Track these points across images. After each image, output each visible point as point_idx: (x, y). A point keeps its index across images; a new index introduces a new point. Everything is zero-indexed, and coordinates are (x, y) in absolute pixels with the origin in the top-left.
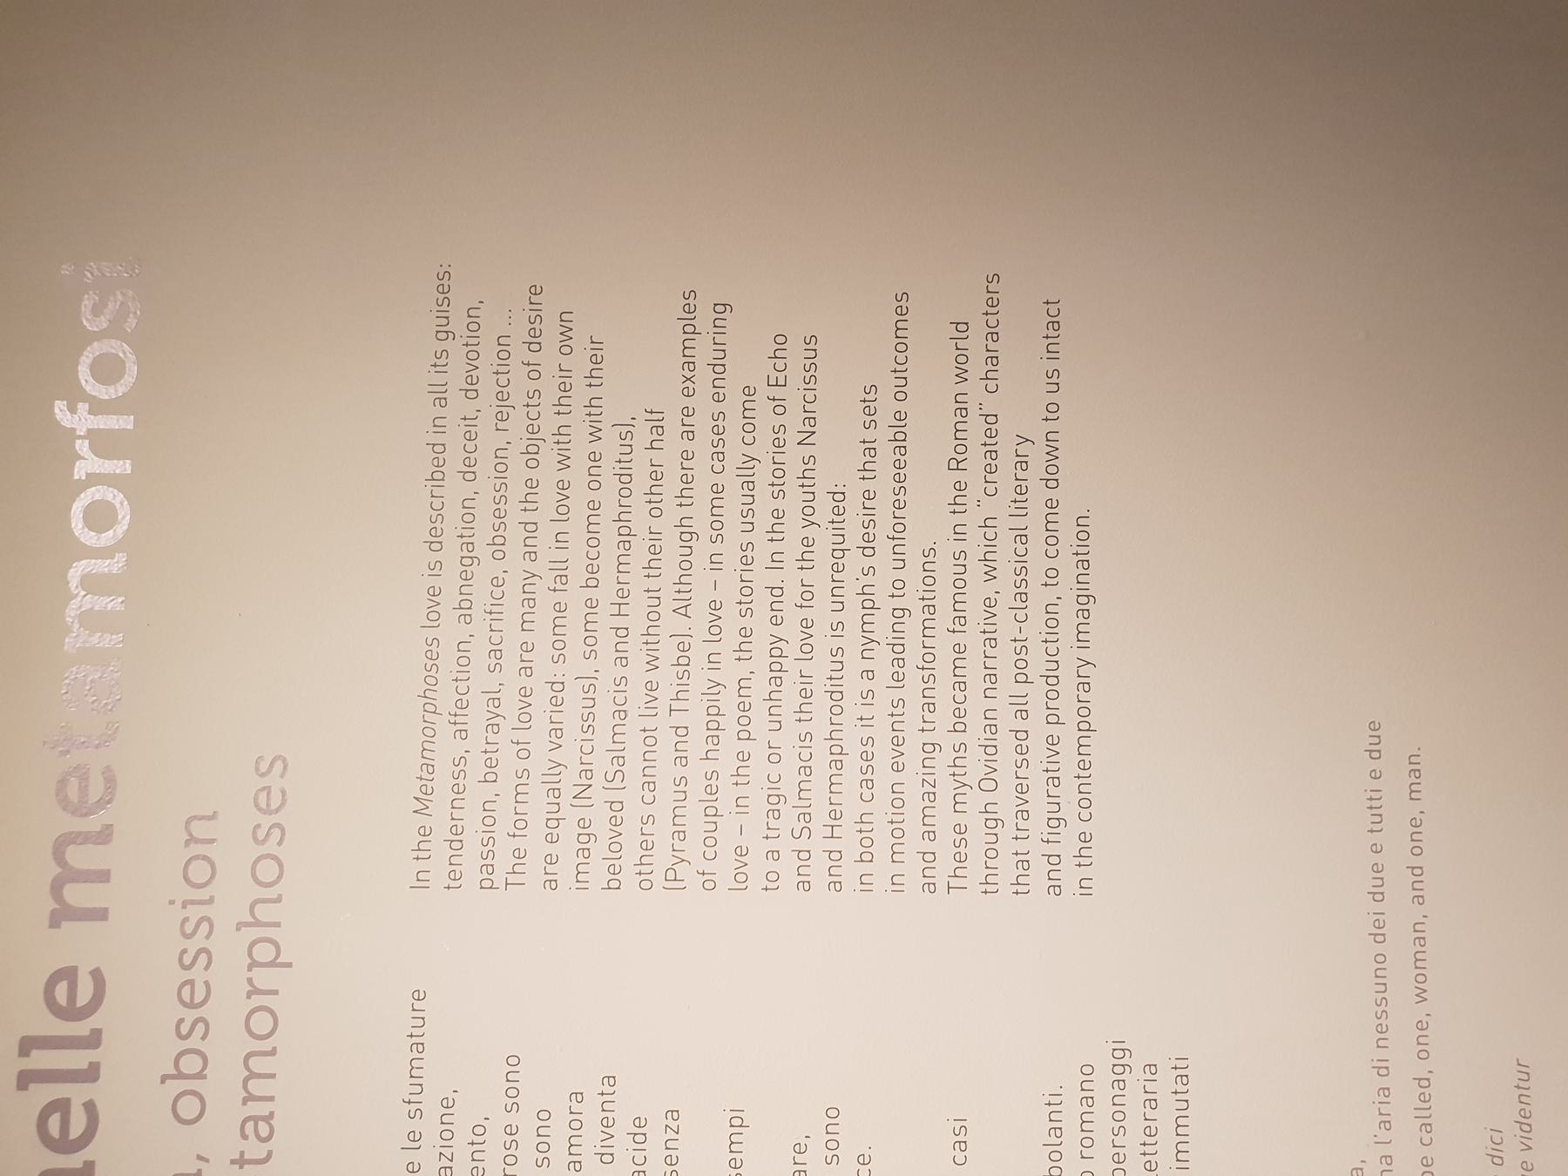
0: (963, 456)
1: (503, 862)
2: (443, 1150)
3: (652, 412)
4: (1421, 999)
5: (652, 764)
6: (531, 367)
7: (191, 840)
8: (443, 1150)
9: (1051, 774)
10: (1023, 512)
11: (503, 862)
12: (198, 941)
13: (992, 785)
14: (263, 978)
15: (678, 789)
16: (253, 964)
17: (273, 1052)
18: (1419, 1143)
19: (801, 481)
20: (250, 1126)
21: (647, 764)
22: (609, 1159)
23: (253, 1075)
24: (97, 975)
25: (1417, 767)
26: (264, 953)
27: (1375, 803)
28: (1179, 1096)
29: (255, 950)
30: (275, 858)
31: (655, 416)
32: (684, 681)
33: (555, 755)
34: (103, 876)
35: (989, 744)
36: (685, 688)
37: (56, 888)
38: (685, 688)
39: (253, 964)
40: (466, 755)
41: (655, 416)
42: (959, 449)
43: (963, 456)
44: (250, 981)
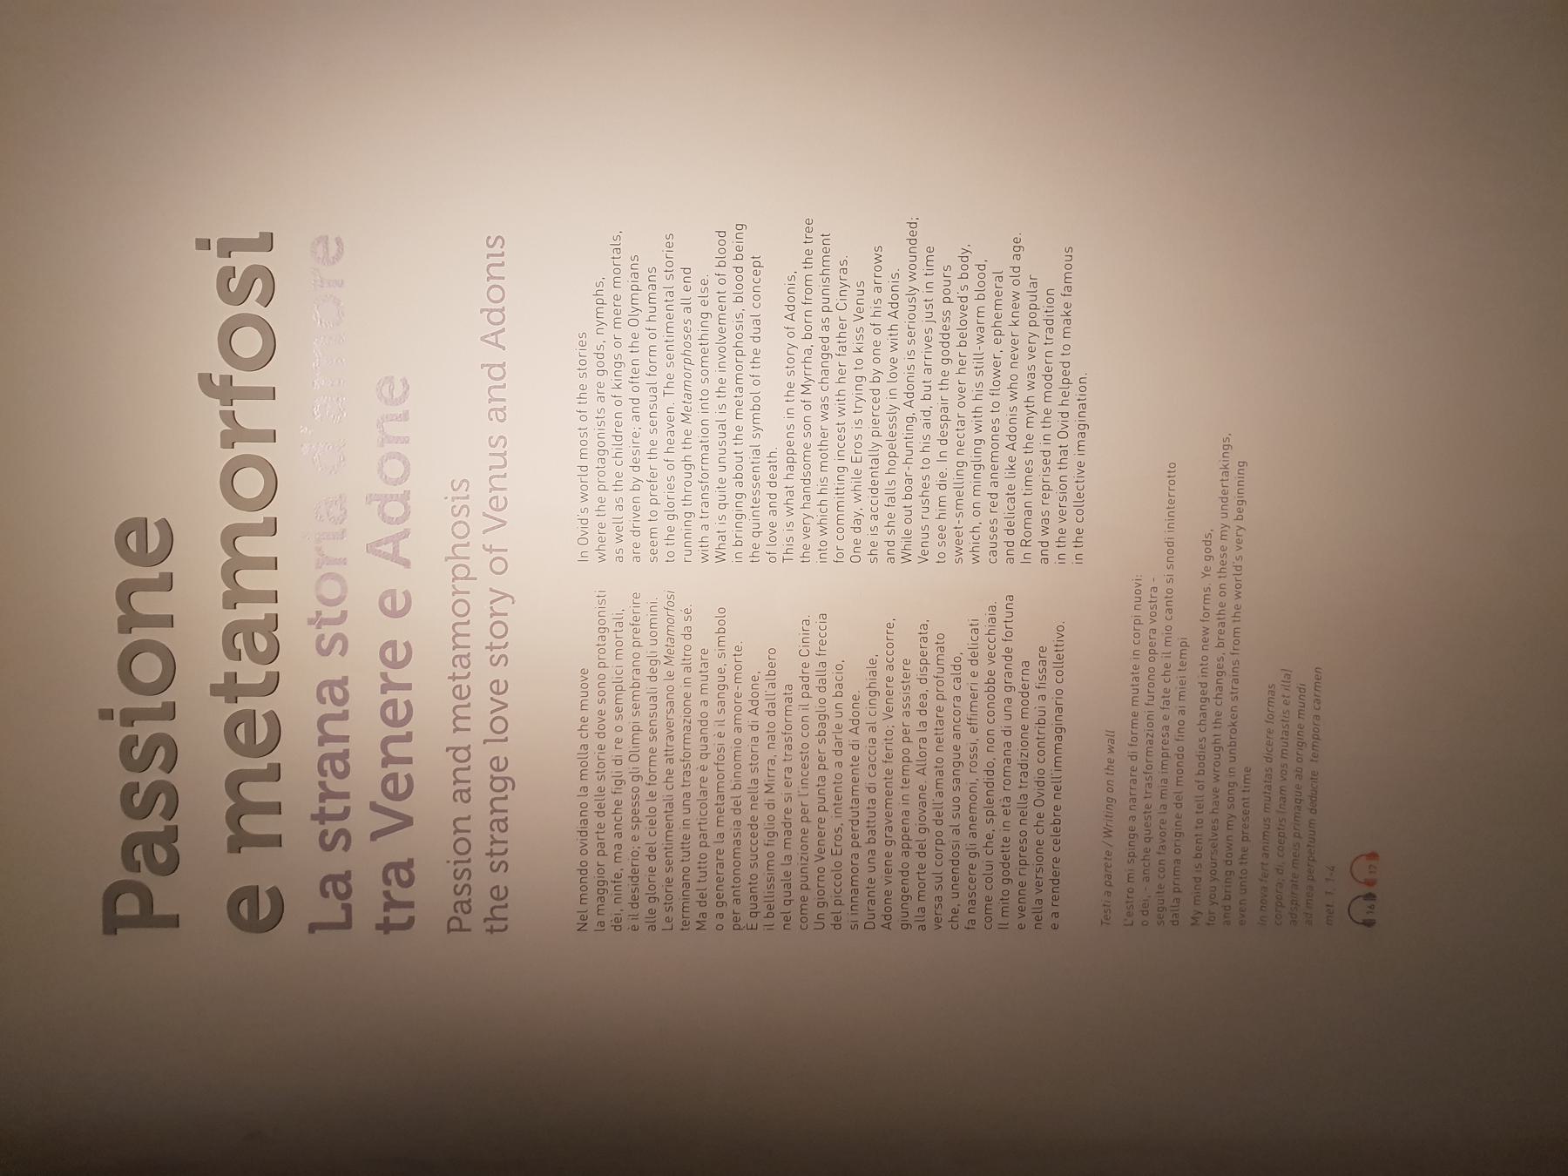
5: (827, 268)
7: (457, 831)
9: (974, 627)
12: (464, 881)
13: (857, 559)
14: (460, 585)
16: (455, 578)
20: (458, 795)
21: (825, 268)
22: (924, 713)
23: (458, 718)
24: (407, 645)
26: (461, 572)
27: (702, 865)
28: (703, 674)
29: (457, 845)
30: (465, 523)
33: (912, 284)
36: (1014, 417)
38: (1014, 417)
39: (455, 578)
40: (620, 234)
42: (704, 476)
44: (453, 586)
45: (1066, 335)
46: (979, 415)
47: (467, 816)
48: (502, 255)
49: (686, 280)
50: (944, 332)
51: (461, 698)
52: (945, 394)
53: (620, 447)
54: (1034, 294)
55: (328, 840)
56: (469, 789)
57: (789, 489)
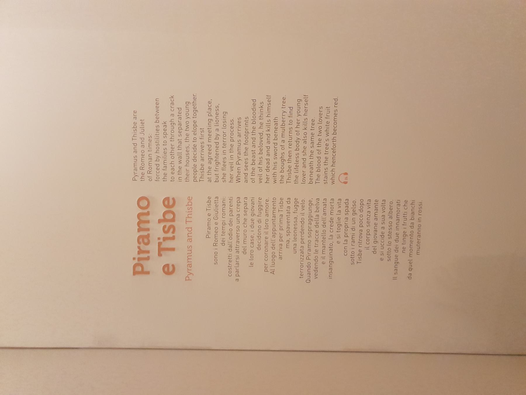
0: (151, 170)
1: (315, 177)
2: (303, 260)
3: (268, 96)
4: (190, 273)
6: (319, 151)
8: (303, 260)
10: (297, 171)
11: (315, 177)
15: (239, 142)
17: (191, 233)
18: (380, 245)
19: (273, 175)
22: (260, 249)
25: (254, 144)
31: (268, 97)
32: (135, 132)
34: (191, 259)
35: (190, 213)
36: (290, 177)
37: (139, 224)
38: (290, 177)
40: (189, 146)
41: (268, 97)
43: (151, 170)
45: (283, 136)
46: (275, 175)
47: (191, 227)
48: (192, 212)
49: (311, 175)
50: (382, 235)
51: (180, 168)
52: (172, 143)
53: (269, 126)
54: (143, 128)
55: (166, 229)
56: (149, 235)
57: (209, 179)
